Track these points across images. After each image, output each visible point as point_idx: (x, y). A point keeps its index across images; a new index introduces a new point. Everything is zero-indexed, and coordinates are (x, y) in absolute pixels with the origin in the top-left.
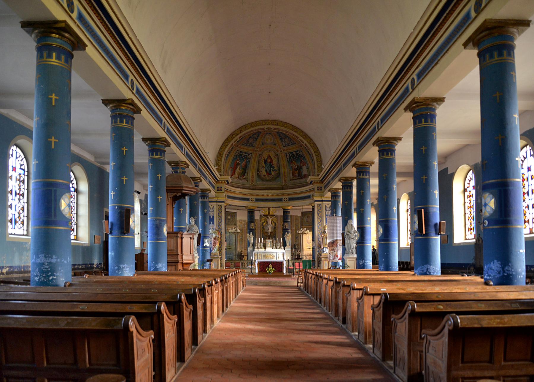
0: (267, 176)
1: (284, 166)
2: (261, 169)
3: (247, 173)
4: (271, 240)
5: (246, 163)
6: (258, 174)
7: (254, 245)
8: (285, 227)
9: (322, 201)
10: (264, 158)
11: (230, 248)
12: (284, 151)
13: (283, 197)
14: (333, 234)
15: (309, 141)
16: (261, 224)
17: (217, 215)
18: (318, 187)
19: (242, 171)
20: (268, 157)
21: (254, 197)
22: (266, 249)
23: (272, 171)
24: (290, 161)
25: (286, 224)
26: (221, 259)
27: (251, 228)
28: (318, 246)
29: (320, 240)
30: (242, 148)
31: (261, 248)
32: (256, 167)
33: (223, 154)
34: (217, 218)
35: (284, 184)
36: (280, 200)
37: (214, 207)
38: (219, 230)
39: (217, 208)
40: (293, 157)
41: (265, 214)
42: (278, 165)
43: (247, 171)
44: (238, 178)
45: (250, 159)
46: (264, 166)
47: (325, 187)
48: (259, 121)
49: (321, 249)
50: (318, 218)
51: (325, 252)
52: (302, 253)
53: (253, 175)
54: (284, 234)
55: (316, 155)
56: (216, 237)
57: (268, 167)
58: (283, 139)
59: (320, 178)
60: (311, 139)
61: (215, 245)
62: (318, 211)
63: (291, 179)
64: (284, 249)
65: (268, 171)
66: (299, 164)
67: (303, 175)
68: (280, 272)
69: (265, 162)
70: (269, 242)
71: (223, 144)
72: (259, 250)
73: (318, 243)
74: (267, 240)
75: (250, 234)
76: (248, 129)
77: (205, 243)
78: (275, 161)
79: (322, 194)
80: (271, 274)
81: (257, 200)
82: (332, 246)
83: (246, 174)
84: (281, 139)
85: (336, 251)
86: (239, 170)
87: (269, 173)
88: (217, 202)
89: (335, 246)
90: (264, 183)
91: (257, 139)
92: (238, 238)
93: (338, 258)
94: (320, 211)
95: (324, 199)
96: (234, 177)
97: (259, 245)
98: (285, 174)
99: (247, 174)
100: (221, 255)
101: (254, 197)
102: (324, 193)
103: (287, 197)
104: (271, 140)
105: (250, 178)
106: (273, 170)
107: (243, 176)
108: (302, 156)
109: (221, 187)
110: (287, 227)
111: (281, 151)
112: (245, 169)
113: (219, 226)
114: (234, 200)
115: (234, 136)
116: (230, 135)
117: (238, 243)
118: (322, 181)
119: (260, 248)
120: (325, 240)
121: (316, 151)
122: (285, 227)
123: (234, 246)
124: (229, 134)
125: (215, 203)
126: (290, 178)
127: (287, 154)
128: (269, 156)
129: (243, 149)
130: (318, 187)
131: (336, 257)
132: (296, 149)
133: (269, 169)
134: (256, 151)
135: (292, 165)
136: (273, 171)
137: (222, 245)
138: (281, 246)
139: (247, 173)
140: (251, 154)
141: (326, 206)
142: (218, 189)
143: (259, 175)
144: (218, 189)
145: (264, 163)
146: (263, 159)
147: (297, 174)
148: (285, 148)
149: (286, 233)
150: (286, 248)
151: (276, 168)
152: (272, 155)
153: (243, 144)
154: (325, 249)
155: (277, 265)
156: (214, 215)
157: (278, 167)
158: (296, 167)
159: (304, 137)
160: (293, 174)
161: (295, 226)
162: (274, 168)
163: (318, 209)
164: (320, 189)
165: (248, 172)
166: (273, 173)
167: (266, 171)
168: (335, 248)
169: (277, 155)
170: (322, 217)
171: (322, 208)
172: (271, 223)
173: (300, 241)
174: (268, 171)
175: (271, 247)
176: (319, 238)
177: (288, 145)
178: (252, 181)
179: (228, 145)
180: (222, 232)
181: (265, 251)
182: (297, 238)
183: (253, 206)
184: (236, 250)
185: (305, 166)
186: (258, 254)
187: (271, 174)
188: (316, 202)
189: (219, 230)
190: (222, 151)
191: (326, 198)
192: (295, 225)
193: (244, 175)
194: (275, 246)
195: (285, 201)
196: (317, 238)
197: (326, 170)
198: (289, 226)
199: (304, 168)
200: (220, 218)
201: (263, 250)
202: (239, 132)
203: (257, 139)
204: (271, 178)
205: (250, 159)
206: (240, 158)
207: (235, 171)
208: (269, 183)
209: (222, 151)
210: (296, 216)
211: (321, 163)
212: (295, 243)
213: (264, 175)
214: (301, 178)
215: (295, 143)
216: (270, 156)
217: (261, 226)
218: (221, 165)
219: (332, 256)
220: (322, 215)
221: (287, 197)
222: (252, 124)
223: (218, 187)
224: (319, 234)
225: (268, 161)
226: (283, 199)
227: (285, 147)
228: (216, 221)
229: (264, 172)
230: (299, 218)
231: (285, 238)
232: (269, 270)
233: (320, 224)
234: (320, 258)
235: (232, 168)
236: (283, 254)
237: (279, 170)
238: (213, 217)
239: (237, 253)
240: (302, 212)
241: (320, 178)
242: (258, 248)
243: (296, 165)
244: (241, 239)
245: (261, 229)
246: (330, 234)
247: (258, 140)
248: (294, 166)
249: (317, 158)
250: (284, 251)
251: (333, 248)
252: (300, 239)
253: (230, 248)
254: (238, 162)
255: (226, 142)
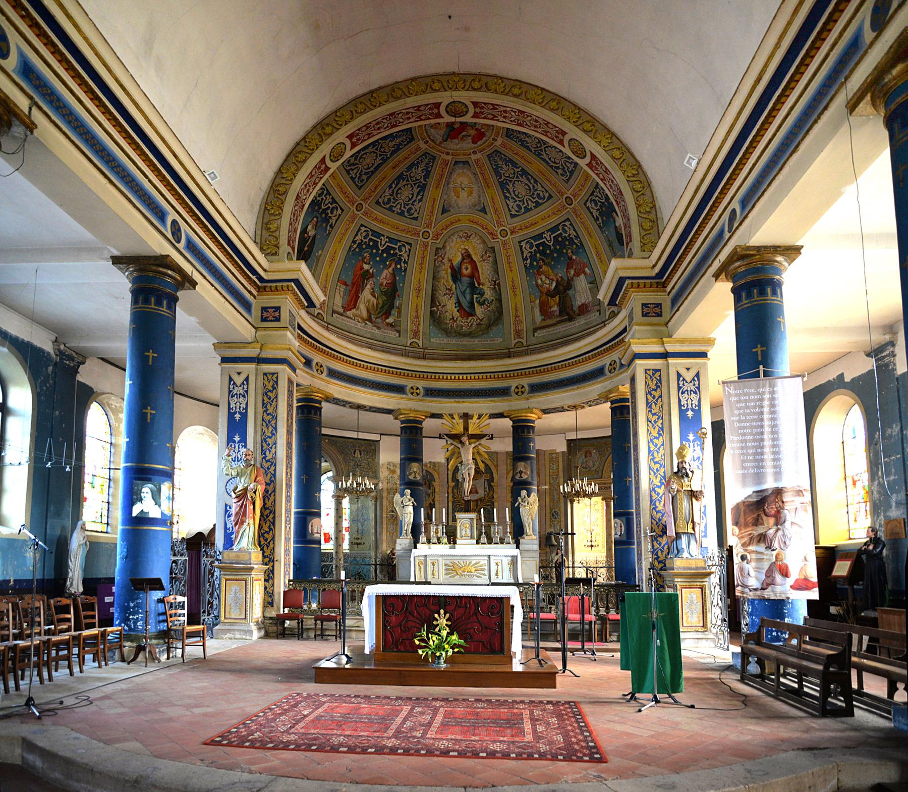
0: (461, 321)
1: (514, 288)
2: (444, 299)
3: (398, 308)
4: (473, 515)
5: (394, 275)
6: (432, 313)
7: (415, 532)
8: (517, 477)
9: (665, 355)
10: (450, 260)
11: (360, 544)
12: (512, 233)
13: (513, 383)
14: (759, 463)
15: (605, 143)
16: (450, 477)
17: (260, 409)
18: (644, 305)
19: (380, 301)
20: (463, 259)
21: (421, 384)
22: (455, 543)
23: (476, 304)
24: (532, 268)
25: (521, 466)
26: (269, 576)
27: (411, 477)
28: (652, 530)
29: (660, 507)
30: (376, 219)
31: (438, 539)
32: (426, 293)
33: (286, 193)
34: (260, 420)
35: (514, 342)
36: (504, 392)
37: (247, 379)
38: (266, 465)
39: (260, 385)
40: (543, 253)
41: (454, 432)
42: (496, 286)
43: (397, 303)
44: (369, 319)
45: (405, 262)
46: (450, 290)
47: (674, 301)
48: (421, 77)
49: (664, 541)
50: (648, 421)
51: (685, 555)
52: (570, 558)
53: (417, 317)
54: (515, 494)
55: (634, 190)
56: (245, 490)
57: (463, 293)
58: (510, 187)
59: (654, 266)
60: (613, 135)
61: (243, 523)
62: (648, 393)
63: (538, 325)
64: (518, 547)
65: (465, 304)
66: (561, 272)
67: (575, 309)
68: (492, 651)
69: (456, 274)
70: (465, 521)
71: (288, 156)
72: (432, 546)
73: (652, 517)
74: (459, 515)
75: (402, 495)
76: (381, 104)
77: (141, 500)
78: (485, 271)
79: (664, 328)
80: (443, 666)
81: (430, 393)
82: (757, 522)
83: (394, 312)
84: (503, 186)
85: (776, 545)
86: (370, 297)
87: (468, 312)
88: (259, 360)
89: (772, 521)
90: (454, 341)
91: (423, 188)
92: (384, 515)
93: (790, 581)
94: (657, 394)
95: (670, 348)
96: (355, 315)
97: (433, 529)
98: (516, 311)
99: (399, 312)
100: (269, 559)
101: (421, 384)
102: (670, 324)
103: (525, 382)
104: (470, 193)
105: (407, 324)
106: (478, 302)
107: (387, 318)
108: (571, 241)
109: (278, 309)
110: (525, 477)
111: (504, 233)
112: (391, 294)
113: (263, 452)
114: (353, 387)
115: (328, 130)
116: (314, 127)
117: (382, 528)
118: (660, 280)
119: (435, 540)
120: (685, 503)
121: (634, 175)
122: (517, 477)
123: (373, 538)
124: (311, 122)
125: (252, 366)
126: (534, 322)
127: (523, 244)
128: (467, 256)
129: (381, 221)
130: (644, 305)
131: (778, 578)
132: (554, 220)
133: (468, 297)
134: (426, 234)
135: (539, 281)
136: (481, 304)
137: (273, 523)
138: (505, 533)
139: (399, 308)
140: (410, 244)
141: (679, 375)
142: (265, 314)
143: (436, 319)
144: (265, 314)
145: (450, 278)
146: (448, 265)
147: (556, 308)
148: (517, 222)
149: (524, 493)
150: (521, 541)
151: (489, 294)
152: (476, 249)
153: (378, 203)
154: (684, 539)
155: (476, 613)
156: (246, 409)
157: (495, 289)
158: (554, 284)
159: (587, 126)
160: (544, 310)
161: (547, 481)
162: (482, 294)
163: (647, 385)
164: (652, 311)
165: (401, 304)
166: (479, 310)
167: (459, 303)
168: (772, 531)
169: (493, 249)
170: (666, 418)
171: (664, 383)
172: (471, 461)
173: (563, 524)
174: (465, 304)
175: (472, 537)
176: (655, 496)
177: (527, 210)
178: (416, 334)
179: (304, 161)
180: (274, 475)
181: (452, 552)
182: (554, 515)
183: (415, 411)
184: (377, 547)
185: (582, 276)
186: (425, 561)
187: (474, 315)
188: (638, 362)
189: (266, 465)
190: (283, 181)
191: (682, 341)
192: (547, 478)
193: (388, 314)
194: (485, 535)
195: (517, 393)
196: (648, 498)
197: (677, 226)
198: (532, 472)
199: (581, 283)
200: (269, 421)
201: (443, 549)
202: (348, 117)
203: (425, 185)
204: (474, 327)
205: (405, 262)
206: (371, 254)
207: (358, 297)
208: (466, 341)
209: (283, 181)
210: (552, 453)
211: (652, 216)
212: (549, 530)
213: (453, 318)
214: (571, 319)
215: (550, 197)
216: (469, 256)
217: (450, 480)
218: (278, 228)
219: (757, 569)
220: (665, 407)
221: (525, 382)
222: (393, 90)
223: (264, 309)
224: (657, 482)
225: (464, 271)
226: (513, 388)
227: (516, 219)
228: (255, 432)
229: (450, 308)
230: (561, 459)
231: (518, 508)
232: (434, 640)
233: (659, 442)
234: (660, 576)
235: (345, 284)
236: (514, 561)
237: (500, 300)
238: (244, 416)
239: (379, 556)
240: (570, 442)
241: (654, 266)
242: (429, 541)
243: (553, 280)
244: (393, 516)
245: (450, 490)
246: (743, 461)
247: (430, 192)
248: (548, 282)
249: (637, 199)
250: (516, 552)
251: (760, 530)
252: (563, 519)
253: (359, 541)
254: (366, 267)
255: (300, 152)
